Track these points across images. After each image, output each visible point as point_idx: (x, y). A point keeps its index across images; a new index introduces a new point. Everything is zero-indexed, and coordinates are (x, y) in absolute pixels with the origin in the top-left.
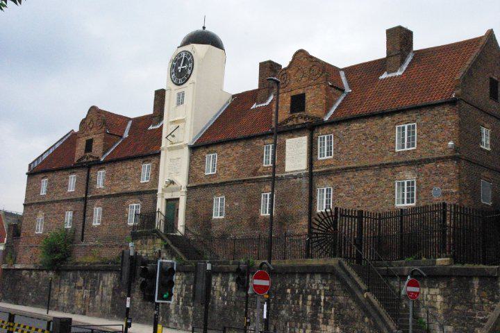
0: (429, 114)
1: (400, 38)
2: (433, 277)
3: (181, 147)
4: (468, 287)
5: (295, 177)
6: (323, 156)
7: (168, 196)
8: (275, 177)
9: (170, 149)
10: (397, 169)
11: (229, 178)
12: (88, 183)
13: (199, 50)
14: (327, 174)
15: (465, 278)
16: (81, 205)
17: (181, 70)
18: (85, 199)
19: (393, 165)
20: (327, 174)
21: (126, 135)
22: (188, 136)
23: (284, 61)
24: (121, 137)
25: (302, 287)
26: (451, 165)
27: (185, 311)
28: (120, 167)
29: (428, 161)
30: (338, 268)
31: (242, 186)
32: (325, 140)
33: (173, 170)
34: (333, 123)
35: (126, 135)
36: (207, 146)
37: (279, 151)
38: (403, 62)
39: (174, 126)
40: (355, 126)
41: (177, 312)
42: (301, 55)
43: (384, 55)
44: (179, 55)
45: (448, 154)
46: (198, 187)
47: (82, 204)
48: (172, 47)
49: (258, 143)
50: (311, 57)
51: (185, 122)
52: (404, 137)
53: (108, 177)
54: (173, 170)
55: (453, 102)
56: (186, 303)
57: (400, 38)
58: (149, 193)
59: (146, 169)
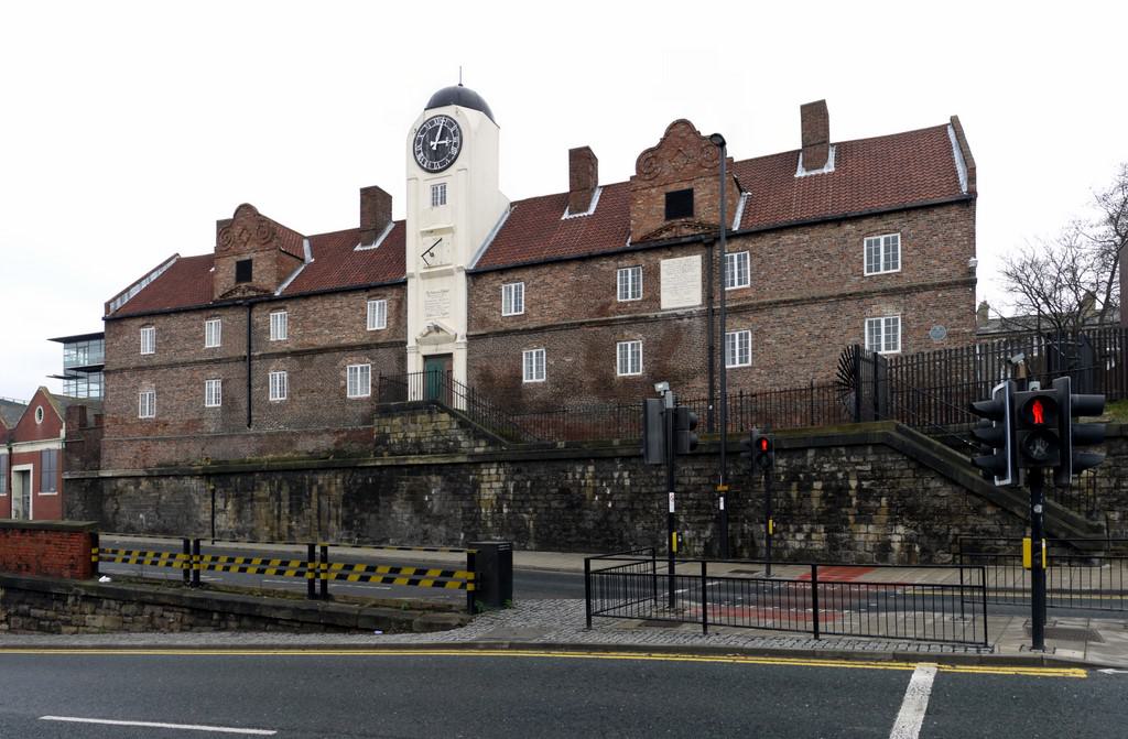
0: (922, 220)
10: (867, 301)
12: (252, 334)
18: (249, 359)
22: (465, 251)
24: (303, 260)
33: (437, 311)
34: (287, 298)
40: (789, 238)
46: (482, 333)
48: (414, 112)
54: (437, 311)
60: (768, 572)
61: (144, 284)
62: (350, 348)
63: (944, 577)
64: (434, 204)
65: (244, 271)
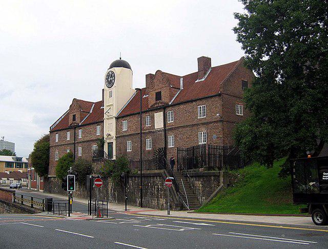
0: (210, 100)
1: (204, 62)
2: (198, 176)
3: (112, 118)
4: (209, 181)
5: (159, 131)
6: (170, 121)
7: (108, 141)
8: (152, 132)
9: (108, 119)
10: (199, 127)
11: (133, 132)
12: (75, 136)
13: (117, 70)
14: (171, 129)
15: (213, 178)
16: (138, 138)
17: (110, 80)
18: (75, 143)
19: (197, 125)
20: (171, 129)
21: (91, 112)
22: (114, 113)
23: (241, 44)
24: (179, 89)
25: (154, 182)
26: (220, 124)
27: (115, 194)
28: (88, 128)
29: (211, 123)
30: (167, 175)
31: (141, 134)
32: (169, 112)
33: (109, 129)
34: (172, 106)
35: (91, 112)
36: (123, 117)
37: (153, 118)
38: (205, 74)
39: (109, 108)
40: (182, 106)
41: (111, 195)
42: (149, 77)
43: (197, 71)
44: (109, 73)
45: (218, 119)
46: (120, 137)
47: (73, 145)
48: (105, 69)
49: (144, 115)
50: (164, 73)
51: (113, 108)
52: (201, 111)
53: (83, 133)
54: (109, 129)
55: (220, 95)
56: (114, 191)
57: (204, 62)
58: (101, 142)
59: (99, 128)
60: (169, 214)
61: (61, 119)
62: (92, 141)
63: (138, 210)
64: (110, 97)
65: (158, 96)
